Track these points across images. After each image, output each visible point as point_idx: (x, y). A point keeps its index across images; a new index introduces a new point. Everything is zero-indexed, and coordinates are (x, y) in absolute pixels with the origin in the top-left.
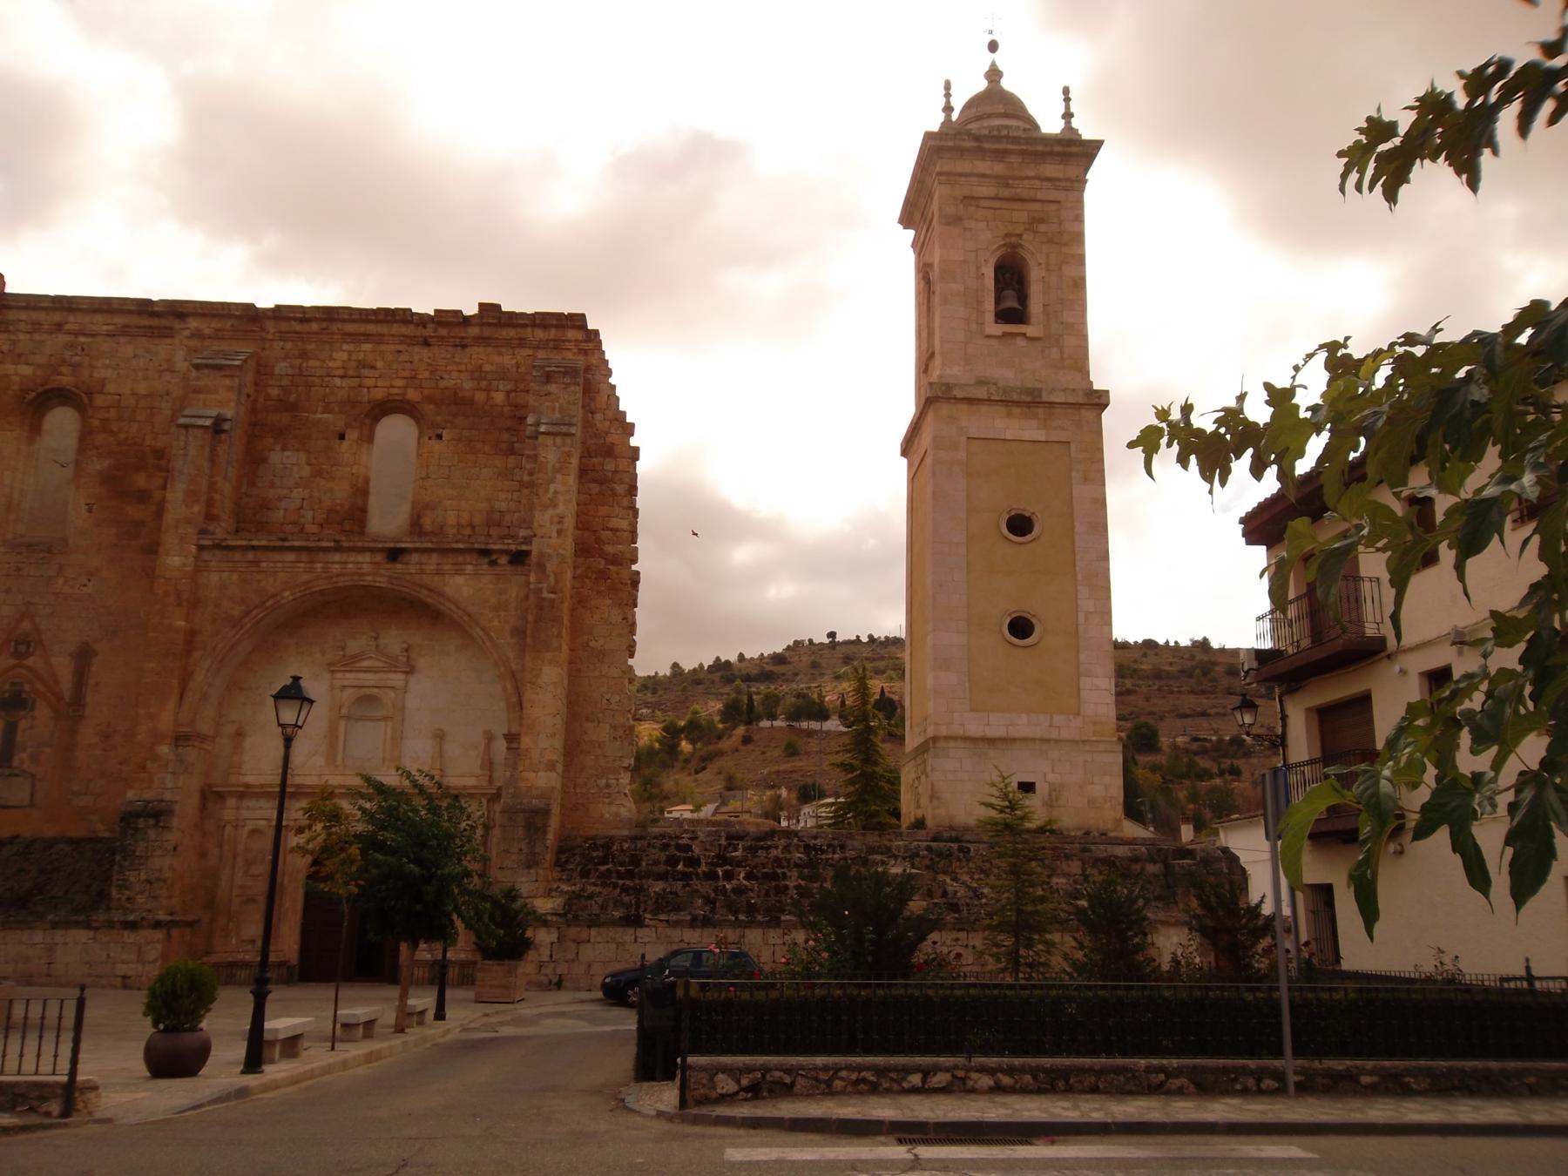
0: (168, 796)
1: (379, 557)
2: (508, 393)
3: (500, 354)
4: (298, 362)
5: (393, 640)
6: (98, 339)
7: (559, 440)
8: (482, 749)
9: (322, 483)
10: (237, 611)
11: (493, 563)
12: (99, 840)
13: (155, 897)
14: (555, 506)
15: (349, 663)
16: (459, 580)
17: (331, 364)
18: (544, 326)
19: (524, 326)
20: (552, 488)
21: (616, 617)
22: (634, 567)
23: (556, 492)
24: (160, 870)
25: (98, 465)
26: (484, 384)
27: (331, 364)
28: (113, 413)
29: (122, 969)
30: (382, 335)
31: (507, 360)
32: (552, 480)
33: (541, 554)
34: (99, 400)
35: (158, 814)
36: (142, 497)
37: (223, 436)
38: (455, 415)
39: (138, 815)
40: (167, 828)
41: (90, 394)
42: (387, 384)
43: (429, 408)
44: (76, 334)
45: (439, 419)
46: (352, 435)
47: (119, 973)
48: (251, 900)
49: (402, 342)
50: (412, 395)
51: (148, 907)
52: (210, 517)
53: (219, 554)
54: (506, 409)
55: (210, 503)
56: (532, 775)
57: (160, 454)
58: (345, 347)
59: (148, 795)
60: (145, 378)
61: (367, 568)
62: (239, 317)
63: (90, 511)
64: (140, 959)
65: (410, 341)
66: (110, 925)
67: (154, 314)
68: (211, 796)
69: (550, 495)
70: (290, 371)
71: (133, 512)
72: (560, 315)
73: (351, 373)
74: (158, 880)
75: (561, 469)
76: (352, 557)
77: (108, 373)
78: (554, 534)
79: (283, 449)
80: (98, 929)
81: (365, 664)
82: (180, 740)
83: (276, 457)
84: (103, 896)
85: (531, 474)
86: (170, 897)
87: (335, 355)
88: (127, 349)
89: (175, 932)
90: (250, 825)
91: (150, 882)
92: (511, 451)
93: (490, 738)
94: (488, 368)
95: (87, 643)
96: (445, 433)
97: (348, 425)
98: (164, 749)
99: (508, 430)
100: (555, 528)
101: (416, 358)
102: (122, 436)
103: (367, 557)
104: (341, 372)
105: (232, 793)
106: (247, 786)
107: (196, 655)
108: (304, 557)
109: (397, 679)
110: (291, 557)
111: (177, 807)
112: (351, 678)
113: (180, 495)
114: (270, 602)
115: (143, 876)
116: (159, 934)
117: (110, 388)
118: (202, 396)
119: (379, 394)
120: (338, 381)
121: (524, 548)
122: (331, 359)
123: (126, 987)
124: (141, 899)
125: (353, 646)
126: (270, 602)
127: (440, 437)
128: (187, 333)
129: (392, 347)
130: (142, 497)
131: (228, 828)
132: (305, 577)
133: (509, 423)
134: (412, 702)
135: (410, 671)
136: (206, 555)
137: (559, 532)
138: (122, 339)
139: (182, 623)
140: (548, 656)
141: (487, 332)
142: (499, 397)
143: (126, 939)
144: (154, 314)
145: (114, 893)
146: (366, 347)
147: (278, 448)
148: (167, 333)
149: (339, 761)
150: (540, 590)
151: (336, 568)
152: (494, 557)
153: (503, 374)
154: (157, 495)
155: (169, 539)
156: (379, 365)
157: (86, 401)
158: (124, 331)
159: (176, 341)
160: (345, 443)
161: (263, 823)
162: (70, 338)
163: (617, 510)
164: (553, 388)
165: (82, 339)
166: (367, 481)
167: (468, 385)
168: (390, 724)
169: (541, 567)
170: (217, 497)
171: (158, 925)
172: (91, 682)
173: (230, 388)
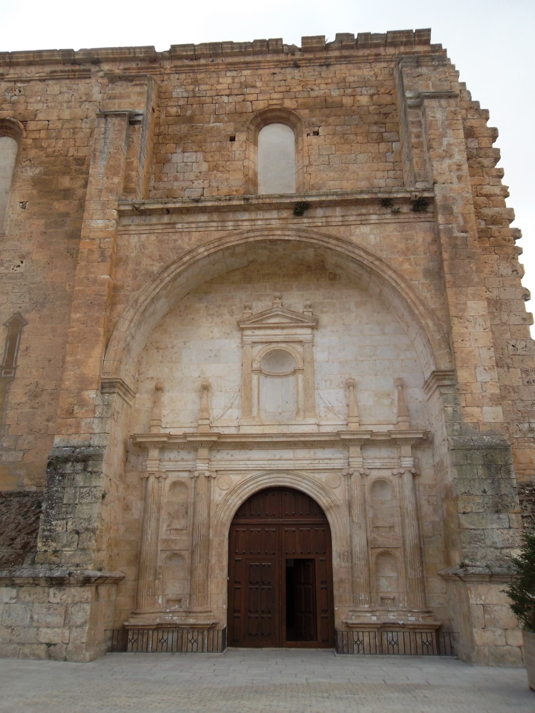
0: (96, 441)
1: (285, 214)
2: (371, 96)
3: (359, 68)
4: (191, 87)
5: (296, 300)
6: (32, 83)
7: (443, 102)
8: (396, 397)
9: (219, 175)
10: (156, 268)
11: (396, 212)
12: (26, 494)
13: (83, 549)
14: (451, 156)
15: (259, 321)
16: (365, 229)
17: (219, 87)
18: (394, 45)
19: (377, 46)
20: (445, 141)
21: (505, 269)
22: (512, 226)
23: (449, 145)
24: (89, 520)
25: (30, 173)
26: (349, 91)
27: (219, 87)
28: (43, 134)
29: (46, 635)
30: (259, 62)
31: (366, 72)
32: (444, 135)
33: (445, 198)
34: (31, 125)
35: (86, 459)
36: (67, 194)
37: (137, 126)
38: (328, 116)
39: (66, 460)
40: (96, 473)
41: (24, 122)
42: (267, 97)
43: (304, 113)
44: (15, 82)
45: (314, 119)
46: (241, 137)
47: (44, 639)
48: (175, 555)
49: (276, 67)
50: (288, 104)
51: (77, 560)
52: (128, 190)
53: (137, 220)
54: (372, 108)
55: (127, 179)
56: (476, 410)
57: (81, 161)
58: (229, 74)
59: (75, 441)
60: (69, 108)
61: (275, 223)
62: (142, 60)
63: (24, 207)
64: (67, 624)
65: (282, 65)
66: (35, 582)
67: (74, 62)
68: (136, 447)
69: (444, 147)
70: (185, 95)
71: (59, 206)
72: (408, 33)
73: (236, 92)
74: (87, 529)
75: (450, 125)
76: (261, 215)
77: (39, 106)
78: (455, 180)
79: (183, 152)
80: (21, 586)
81: (272, 321)
82: (108, 386)
83: (177, 158)
84: (28, 548)
85: (418, 136)
86: (99, 550)
87: (221, 80)
88: (54, 88)
89: (103, 590)
90: (173, 477)
91: (78, 533)
92: (381, 140)
93: (401, 385)
94: (351, 79)
95: (19, 313)
96: (321, 130)
97: (236, 130)
98: (91, 394)
99: (376, 123)
100: (454, 175)
101: (289, 77)
102: (50, 150)
103: (274, 214)
104: (227, 92)
105: (155, 444)
106: (169, 436)
107: (120, 307)
108: (215, 217)
109: (304, 334)
110: (203, 218)
111: (105, 452)
112: (261, 334)
113: (102, 170)
114: (187, 258)
115: (70, 527)
116: (87, 593)
117: (40, 116)
118: (116, 101)
119: (261, 105)
120: (225, 99)
121: (426, 195)
122: (218, 83)
123: (50, 657)
124: (68, 552)
125: (259, 306)
126: (187, 258)
127: (316, 133)
128: (101, 74)
129: (268, 71)
130: (67, 194)
131: (152, 479)
132: (217, 235)
133: (376, 118)
134: (320, 355)
135: (315, 326)
136: (125, 221)
137: (459, 178)
138: (50, 82)
139: (107, 277)
140: (470, 290)
141: (345, 53)
142: (364, 100)
143: (52, 599)
144: (74, 62)
145: (40, 545)
146: (246, 72)
147: (179, 150)
148: (85, 75)
149: (255, 414)
150: (450, 231)
151: (246, 226)
152: (396, 207)
153: (365, 83)
154: (79, 192)
155: (92, 206)
156: (259, 84)
157: (22, 126)
158: (53, 76)
159: (93, 81)
160: (236, 143)
161: (186, 474)
162: (12, 84)
163: (487, 179)
164: (424, 70)
165: (19, 85)
166: (256, 174)
167: (335, 93)
168: (300, 376)
169: (448, 210)
170: (134, 173)
171: (86, 581)
172: (22, 347)
173: (140, 94)
